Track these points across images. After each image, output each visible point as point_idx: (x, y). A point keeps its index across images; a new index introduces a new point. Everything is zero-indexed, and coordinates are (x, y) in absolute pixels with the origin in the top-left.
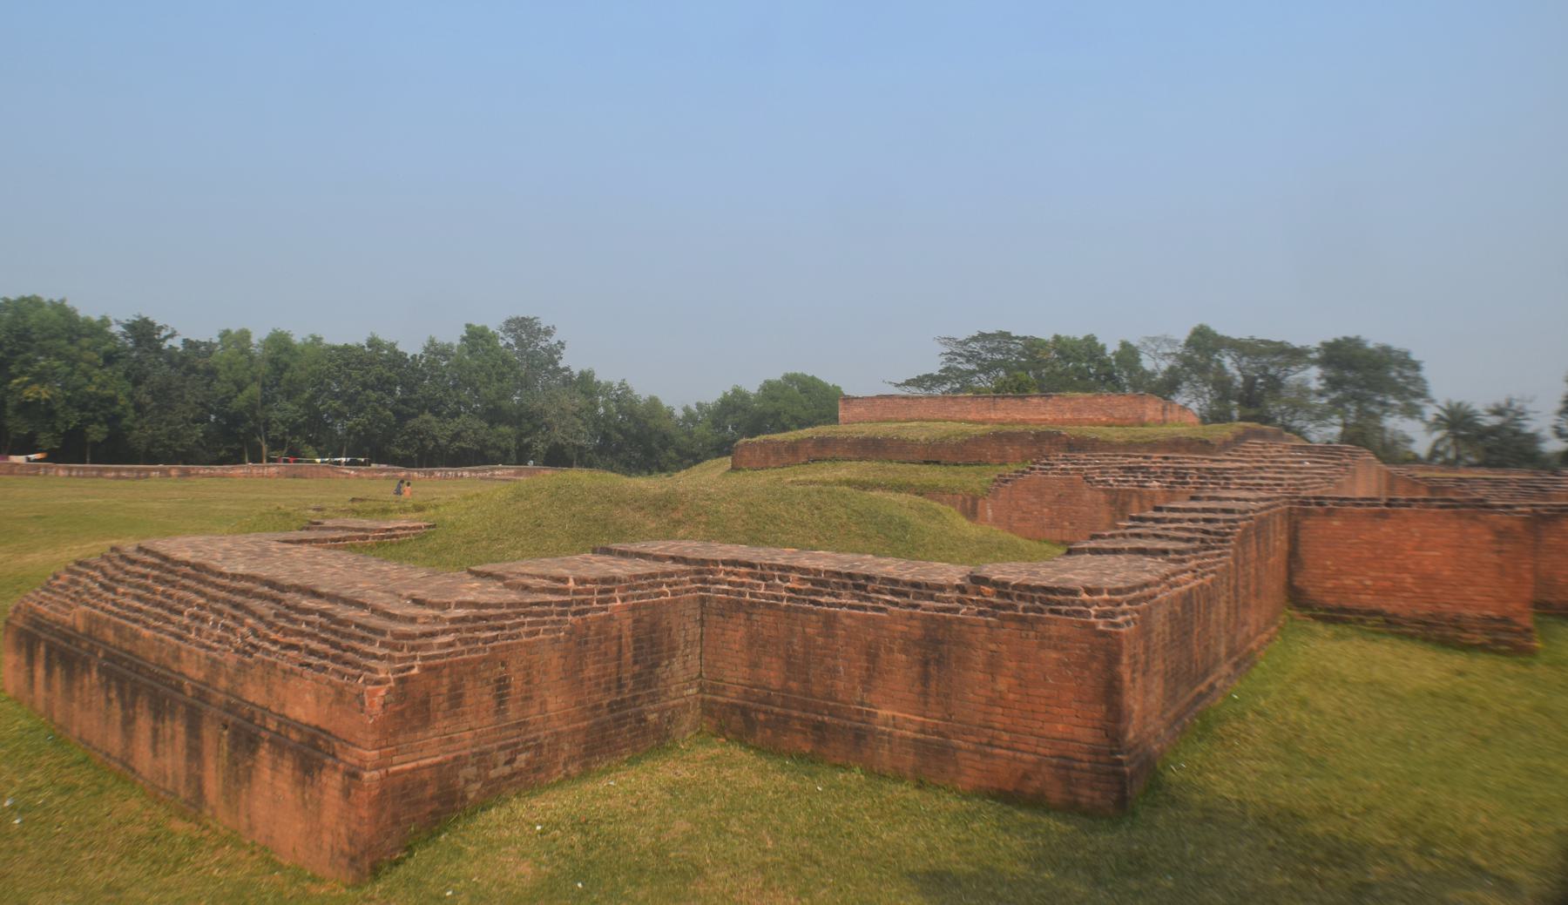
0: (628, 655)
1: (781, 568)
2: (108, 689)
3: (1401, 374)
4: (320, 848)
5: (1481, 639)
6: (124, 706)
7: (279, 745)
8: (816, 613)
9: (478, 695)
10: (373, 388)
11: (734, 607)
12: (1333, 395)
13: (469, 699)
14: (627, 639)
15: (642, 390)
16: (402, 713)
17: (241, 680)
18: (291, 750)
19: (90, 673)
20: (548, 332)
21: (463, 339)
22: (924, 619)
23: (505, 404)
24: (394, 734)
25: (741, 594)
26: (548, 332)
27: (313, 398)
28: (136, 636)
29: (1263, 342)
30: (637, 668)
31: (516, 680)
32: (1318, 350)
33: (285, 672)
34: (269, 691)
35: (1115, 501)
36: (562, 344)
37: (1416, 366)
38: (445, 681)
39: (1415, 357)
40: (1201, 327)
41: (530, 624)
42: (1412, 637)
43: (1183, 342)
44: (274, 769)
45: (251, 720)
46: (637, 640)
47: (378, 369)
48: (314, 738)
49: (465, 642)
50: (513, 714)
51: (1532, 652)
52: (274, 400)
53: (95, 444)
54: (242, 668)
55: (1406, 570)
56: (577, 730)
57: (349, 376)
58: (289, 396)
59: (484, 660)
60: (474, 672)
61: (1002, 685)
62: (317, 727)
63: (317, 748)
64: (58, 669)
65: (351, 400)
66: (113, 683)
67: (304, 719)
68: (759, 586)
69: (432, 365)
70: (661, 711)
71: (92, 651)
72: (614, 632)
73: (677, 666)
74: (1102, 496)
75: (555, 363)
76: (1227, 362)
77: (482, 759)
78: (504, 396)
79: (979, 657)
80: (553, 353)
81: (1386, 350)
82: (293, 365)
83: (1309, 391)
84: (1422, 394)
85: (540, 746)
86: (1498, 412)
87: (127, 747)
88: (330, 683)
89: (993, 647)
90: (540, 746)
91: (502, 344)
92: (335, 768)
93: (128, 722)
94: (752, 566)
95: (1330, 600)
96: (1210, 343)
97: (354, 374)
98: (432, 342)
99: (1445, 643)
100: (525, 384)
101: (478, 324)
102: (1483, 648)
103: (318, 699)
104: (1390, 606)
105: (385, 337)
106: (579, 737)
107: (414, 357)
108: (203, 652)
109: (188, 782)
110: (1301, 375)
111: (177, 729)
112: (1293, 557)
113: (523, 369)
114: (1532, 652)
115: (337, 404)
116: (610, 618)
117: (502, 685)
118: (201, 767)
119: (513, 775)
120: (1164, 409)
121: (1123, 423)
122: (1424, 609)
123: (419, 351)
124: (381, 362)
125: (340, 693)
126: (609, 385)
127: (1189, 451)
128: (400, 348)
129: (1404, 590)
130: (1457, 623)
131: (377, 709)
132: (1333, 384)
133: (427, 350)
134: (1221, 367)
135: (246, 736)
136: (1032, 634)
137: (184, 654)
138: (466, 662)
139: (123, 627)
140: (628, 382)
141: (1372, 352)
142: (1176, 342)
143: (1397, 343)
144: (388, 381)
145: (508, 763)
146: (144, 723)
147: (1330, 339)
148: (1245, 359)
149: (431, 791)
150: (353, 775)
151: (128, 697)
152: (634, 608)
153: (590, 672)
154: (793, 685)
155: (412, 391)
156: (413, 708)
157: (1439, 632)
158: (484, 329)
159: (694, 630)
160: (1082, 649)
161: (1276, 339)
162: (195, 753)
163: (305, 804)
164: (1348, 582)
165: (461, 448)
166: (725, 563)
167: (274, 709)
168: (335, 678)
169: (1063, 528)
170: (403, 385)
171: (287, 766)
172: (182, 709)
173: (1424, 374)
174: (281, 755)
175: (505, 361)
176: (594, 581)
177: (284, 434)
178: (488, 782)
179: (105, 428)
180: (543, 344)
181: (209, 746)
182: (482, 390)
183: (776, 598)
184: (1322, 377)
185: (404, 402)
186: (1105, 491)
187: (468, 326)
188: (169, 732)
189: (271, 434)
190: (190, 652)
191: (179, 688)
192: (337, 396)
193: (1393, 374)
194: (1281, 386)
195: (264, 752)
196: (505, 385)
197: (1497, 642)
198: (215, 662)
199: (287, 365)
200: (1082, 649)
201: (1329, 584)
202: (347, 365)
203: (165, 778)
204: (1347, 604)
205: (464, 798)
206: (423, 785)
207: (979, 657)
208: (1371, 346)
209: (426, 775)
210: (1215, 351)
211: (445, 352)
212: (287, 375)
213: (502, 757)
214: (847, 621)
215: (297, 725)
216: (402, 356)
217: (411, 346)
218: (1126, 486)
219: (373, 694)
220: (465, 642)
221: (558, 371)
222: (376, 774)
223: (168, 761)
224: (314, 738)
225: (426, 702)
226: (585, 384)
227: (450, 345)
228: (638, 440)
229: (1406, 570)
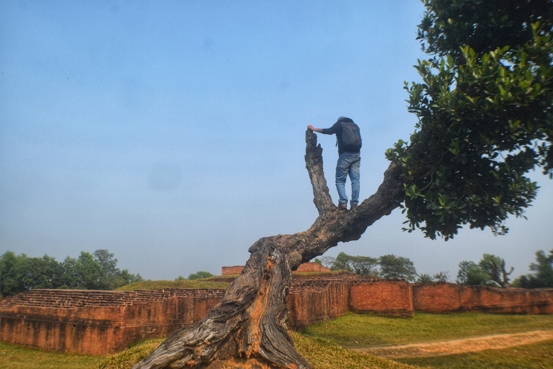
0: (177, 310)
2: (29, 325)
3: (407, 266)
4: (106, 349)
5: (398, 315)
6: (35, 329)
7: (93, 326)
9: (144, 313)
10: (45, 274)
11: (202, 299)
12: (386, 275)
13: (142, 314)
14: (177, 305)
16: (128, 314)
17: (79, 313)
18: (97, 326)
19: (21, 323)
21: (80, 257)
23: (95, 282)
24: (127, 319)
26: (111, 256)
27: (21, 278)
28: (39, 310)
29: (361, 257)
31: (153, 311)
33: (95, 308)
34: (89, 314)
36: (116, 260)
37: (412, 264)
39: (411, 261)
40: (342, 253)
42: (381, 316)
43: (336, 258)
44: (92, 332)
45: (83, 322)
46: (179, 306)
47: (48, 267)
48: (104, 322)
49: (141, 300)
50: (151, 319)
51: (412, 317)
52: (6, 278)
54: (80, 310)
55: (379, 298)
56: (166, 326)
57: (36, 270)
58: (12, 276)
59: (146, 304)
60: (144, 307)
62: (105, 320)
63: (106, 324)
64: (6, 325)
65: (36, 279)
66: (31, 324)
67: (101, 319)
69: (67, 267)
70: (185, 325)
71: (21, 317)
73: (188, 315)
75: (113, 267)
76: (350, 264)
77: (145, 328)
78: (94, 278)
80: (113, 264)
81: (402, 259)
82: (14, 265)
83: (377, 273)
84: (414, 273)
85: (158, 328)
86: (438, 277)
87: (35, 340)
88: (110, 308)
90: (158, 328)
91: (94, 260)
92: (112, 328)
94: (207, 290)
95: (360, 308)
96: (345, 259)
97: (38, 268)
98: (68, 258)
99: (389, 317)
100: (101, 274)
101: (86, 252)
102: (399, 317)
103: (106, 313)
104: (376, 308)
105: (51, 255)
106: (167, 327)
107: (61, 263)
108: (66, 309)
109: (59, 344)
110: (375, 268)
111: (57, 331)
112: (349, 297)
113: (101, 269)
114: (412, 317)
115: (31, 280)
116: (173, 299)
117: (149, 311)
119: (152, 334)
120: (320, 268)
121: (308, 271)
122: (384, 308)
123: (63, 261)
124: (48, 265)
125: (113, 310)
126: (133, 276)
128: (56, 260)
129: (378, 304)
130: (392, 311)
131: (123, 312)
132: (385, 271)
133: (66, 261)
134: (349, 266)
135: (81, 327)
137: (59, 311)
138: (142, 304)
139: (34, 308)
140: (140, 275)
141: (397, 259)
142: (333, 258)
143: (405, 256)
144: (51, 272)
145: (151, 330)
147: (383, 255)
148: (356, 263)
149: (134, 334)
150: (118, 328)
151: (37, 326)
152: (179, 298)
155: (60, 276)
156: (131, 314)
157: (388, 314)
158: (88, 254)
159: (192, 306)
161: (366, 256)
163: (101, 339)
164: (364, 303)
167: (91, 318)
168: (111, 307)
170: (56, 274)
171: (96, 331)
172: (58, 325)
173: (414, 266)
174: (94, 328)
175: (95, 266)
177: (9, 291)
178: (147, 334)
180: (109, 260)
182: (86, 276)
184: (382, 268)
185: (56, 280)
187: (82, 252)
188: (53, 332)
189: (4, 291)
190: (61, 310)
191: (57, 320)
192: (30, 277)
193: (405, 267)
194: (368, 272)
195: (88, 329)
196: (95, 274)
197: (402, 315)
198: (70, 311)
199: (12, 265)
201: (359, 304)
202: (36, 265)
203: (51, 345)
204: (364, 309)
205: (141, 337)
206: (133, 332)
208: (397, 257)
209: (134, 329)
210: (346, 261)
211: (72, 262)
212: (12, 268)
213: (150, 329)
215: (99, 321)
216: (56, 263)
217: (60, 259)
219: (122, 308)
220: (141, 300)
221: (115, 270)
222: (123, 327)
223: (52, 340)
224: (104, 322)
225: (133, 312)
227: (74, 259)
229: (379, 298)
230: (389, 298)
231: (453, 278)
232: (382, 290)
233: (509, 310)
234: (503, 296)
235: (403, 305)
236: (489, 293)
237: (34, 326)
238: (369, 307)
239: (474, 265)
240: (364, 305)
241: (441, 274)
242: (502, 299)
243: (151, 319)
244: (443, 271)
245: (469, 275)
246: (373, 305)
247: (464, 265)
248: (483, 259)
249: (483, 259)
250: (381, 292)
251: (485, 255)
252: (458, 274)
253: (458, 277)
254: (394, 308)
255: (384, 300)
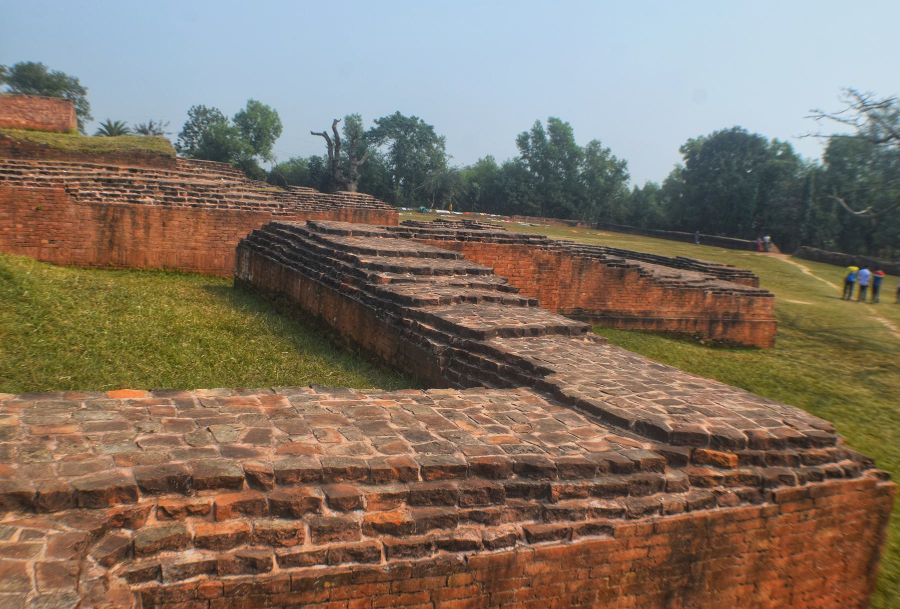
1: (325, 476)
8: (467, 567)
22: (675, 529)
25: (253, 565)
32: (11, 70)
35: (105, 215)
37: (82, 91)
39: (82, 84)
68: (294, 534)
74: (89, 211)
79: (744, 563)
81: (61, 76)
86: (143, 131)
89: (763, 544)
101: (684, 142)
127: (149, 164)
136: (812, 512)
143: (70, 72)
160: (858, 517)
165: (69, 525)
169: (41, 246)
173: (86, 97)
183: (356, 555)
186: (92, 205)
200: (858, 517)
207: (744, 563)
208: (49, 71)
214: (533, 568)
218: (115, 201)
231: (172, 135)
233: (673, 327)
234: (665, 291)
239: (219, 118)
241: (151, 126)
242: (662, 301)
244: (156, 120)
245: (206, 136)
247: (198, 112)
248: (245, 109)
249: (245, 109)
251: (251, 102)
252: (182, 130)
253: (180, 135)
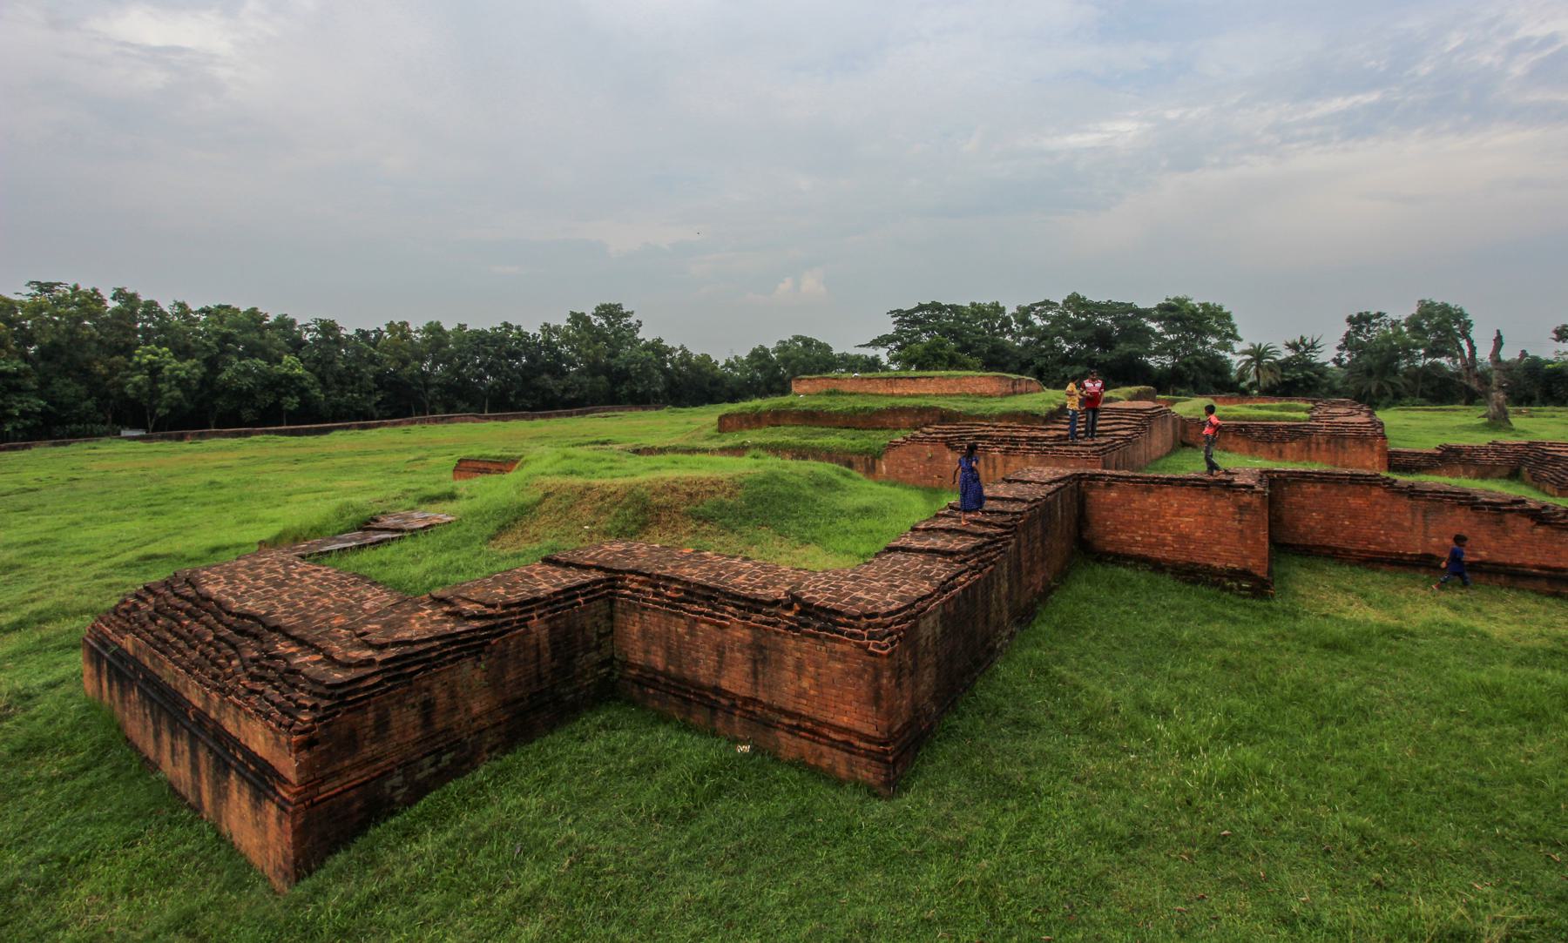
15: (696, 351)
20: (627, 315)
26: (627, 315)
30: (555, 664)
36: (640, 323)
38: (371, 715)
41: (454, 652)
53: (290, 413)
55: (1167, 530)
61: (805, 684)
72: (533, 642)
79: (790, 661)
93: (157, 735)
104: (1159, 554)
118: (199, 779)
146: (166, 738)
153: (511, 676)
154: (672, 668)
162: (195, 768)
166: (631, 572)
176: (516, 605)
179: (297, 399)
181: (203, 766)
207: (790, 661)
226: (657, 348)
228: (689, 384)
230: (1198, 534)
232: (1179, 510)
235: (1244, 558)
236: (1540, 530)
237: (122, 685)
238: (1137, 550)
240: (1122, 542)
243: (439, 724)
246: (1151, 546)
250: (1177, 514)
254: (1215, 564)
255: (1183, 538)
